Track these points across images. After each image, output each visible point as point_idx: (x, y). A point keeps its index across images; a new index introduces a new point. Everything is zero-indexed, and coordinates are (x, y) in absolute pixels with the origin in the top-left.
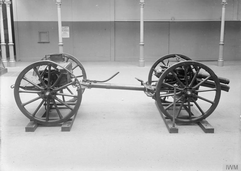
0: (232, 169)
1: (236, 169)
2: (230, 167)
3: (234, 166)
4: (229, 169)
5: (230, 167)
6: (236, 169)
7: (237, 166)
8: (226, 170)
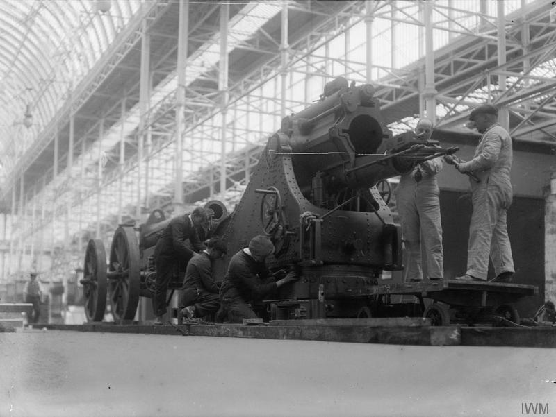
0: (535, 413)
1: (544, 413)
3: (541, 404)
4: (528, 412)
6: (544, 413)
7: (547, 405)
8: (522, 415)
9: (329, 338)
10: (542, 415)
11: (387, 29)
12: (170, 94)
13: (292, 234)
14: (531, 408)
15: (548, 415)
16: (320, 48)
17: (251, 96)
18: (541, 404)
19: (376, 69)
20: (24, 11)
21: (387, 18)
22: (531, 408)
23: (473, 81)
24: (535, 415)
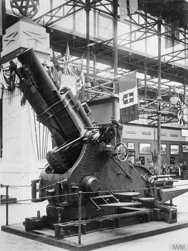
0: (178, 249)
1: (183, 249)
2: (182, 247)
3: (181, 245)
5: (182, 247)
6: (183, 249)
7: (184, 245)
9: (50, 244)
10: (182, 250)
11: (111, 43)
12: (104, 42)
13: (45, 119)
14: (177, 247)
15: (183, 250)
16: (176, 51)
17: (129, 41)
18: (181, 245)
19: (140, 24)
20: (54, 24)
21: (183, 89)
22: (177, 247)
23: (154, 100)
24: (182, 250)
